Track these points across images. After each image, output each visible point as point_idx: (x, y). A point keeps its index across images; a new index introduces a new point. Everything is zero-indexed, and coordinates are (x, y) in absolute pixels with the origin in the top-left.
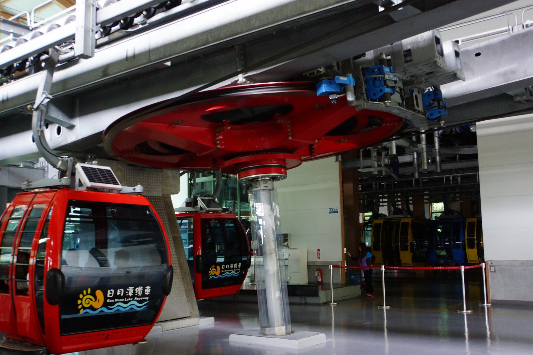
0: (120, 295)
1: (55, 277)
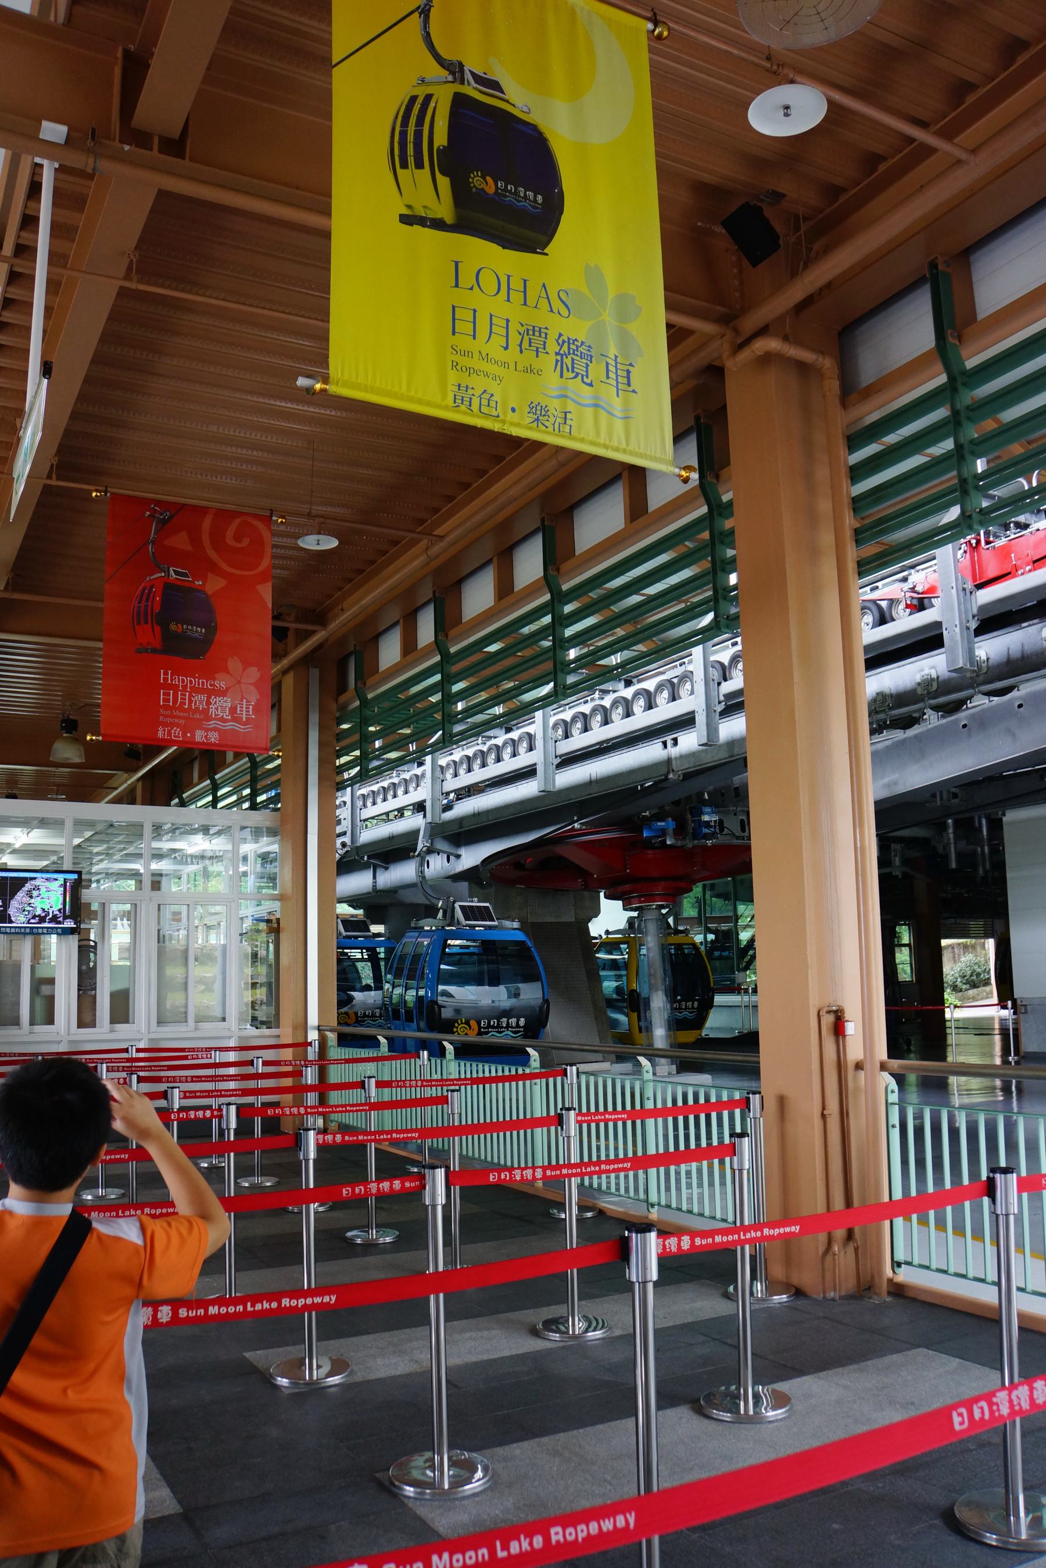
0: (982, 1419)
1: (433, 1008)
